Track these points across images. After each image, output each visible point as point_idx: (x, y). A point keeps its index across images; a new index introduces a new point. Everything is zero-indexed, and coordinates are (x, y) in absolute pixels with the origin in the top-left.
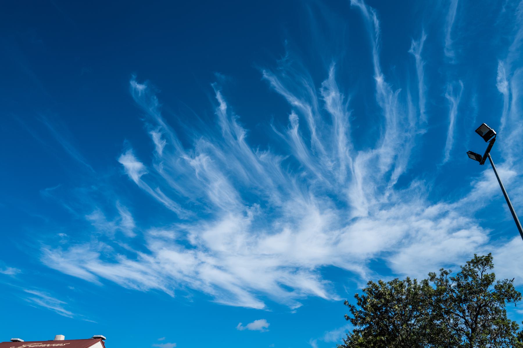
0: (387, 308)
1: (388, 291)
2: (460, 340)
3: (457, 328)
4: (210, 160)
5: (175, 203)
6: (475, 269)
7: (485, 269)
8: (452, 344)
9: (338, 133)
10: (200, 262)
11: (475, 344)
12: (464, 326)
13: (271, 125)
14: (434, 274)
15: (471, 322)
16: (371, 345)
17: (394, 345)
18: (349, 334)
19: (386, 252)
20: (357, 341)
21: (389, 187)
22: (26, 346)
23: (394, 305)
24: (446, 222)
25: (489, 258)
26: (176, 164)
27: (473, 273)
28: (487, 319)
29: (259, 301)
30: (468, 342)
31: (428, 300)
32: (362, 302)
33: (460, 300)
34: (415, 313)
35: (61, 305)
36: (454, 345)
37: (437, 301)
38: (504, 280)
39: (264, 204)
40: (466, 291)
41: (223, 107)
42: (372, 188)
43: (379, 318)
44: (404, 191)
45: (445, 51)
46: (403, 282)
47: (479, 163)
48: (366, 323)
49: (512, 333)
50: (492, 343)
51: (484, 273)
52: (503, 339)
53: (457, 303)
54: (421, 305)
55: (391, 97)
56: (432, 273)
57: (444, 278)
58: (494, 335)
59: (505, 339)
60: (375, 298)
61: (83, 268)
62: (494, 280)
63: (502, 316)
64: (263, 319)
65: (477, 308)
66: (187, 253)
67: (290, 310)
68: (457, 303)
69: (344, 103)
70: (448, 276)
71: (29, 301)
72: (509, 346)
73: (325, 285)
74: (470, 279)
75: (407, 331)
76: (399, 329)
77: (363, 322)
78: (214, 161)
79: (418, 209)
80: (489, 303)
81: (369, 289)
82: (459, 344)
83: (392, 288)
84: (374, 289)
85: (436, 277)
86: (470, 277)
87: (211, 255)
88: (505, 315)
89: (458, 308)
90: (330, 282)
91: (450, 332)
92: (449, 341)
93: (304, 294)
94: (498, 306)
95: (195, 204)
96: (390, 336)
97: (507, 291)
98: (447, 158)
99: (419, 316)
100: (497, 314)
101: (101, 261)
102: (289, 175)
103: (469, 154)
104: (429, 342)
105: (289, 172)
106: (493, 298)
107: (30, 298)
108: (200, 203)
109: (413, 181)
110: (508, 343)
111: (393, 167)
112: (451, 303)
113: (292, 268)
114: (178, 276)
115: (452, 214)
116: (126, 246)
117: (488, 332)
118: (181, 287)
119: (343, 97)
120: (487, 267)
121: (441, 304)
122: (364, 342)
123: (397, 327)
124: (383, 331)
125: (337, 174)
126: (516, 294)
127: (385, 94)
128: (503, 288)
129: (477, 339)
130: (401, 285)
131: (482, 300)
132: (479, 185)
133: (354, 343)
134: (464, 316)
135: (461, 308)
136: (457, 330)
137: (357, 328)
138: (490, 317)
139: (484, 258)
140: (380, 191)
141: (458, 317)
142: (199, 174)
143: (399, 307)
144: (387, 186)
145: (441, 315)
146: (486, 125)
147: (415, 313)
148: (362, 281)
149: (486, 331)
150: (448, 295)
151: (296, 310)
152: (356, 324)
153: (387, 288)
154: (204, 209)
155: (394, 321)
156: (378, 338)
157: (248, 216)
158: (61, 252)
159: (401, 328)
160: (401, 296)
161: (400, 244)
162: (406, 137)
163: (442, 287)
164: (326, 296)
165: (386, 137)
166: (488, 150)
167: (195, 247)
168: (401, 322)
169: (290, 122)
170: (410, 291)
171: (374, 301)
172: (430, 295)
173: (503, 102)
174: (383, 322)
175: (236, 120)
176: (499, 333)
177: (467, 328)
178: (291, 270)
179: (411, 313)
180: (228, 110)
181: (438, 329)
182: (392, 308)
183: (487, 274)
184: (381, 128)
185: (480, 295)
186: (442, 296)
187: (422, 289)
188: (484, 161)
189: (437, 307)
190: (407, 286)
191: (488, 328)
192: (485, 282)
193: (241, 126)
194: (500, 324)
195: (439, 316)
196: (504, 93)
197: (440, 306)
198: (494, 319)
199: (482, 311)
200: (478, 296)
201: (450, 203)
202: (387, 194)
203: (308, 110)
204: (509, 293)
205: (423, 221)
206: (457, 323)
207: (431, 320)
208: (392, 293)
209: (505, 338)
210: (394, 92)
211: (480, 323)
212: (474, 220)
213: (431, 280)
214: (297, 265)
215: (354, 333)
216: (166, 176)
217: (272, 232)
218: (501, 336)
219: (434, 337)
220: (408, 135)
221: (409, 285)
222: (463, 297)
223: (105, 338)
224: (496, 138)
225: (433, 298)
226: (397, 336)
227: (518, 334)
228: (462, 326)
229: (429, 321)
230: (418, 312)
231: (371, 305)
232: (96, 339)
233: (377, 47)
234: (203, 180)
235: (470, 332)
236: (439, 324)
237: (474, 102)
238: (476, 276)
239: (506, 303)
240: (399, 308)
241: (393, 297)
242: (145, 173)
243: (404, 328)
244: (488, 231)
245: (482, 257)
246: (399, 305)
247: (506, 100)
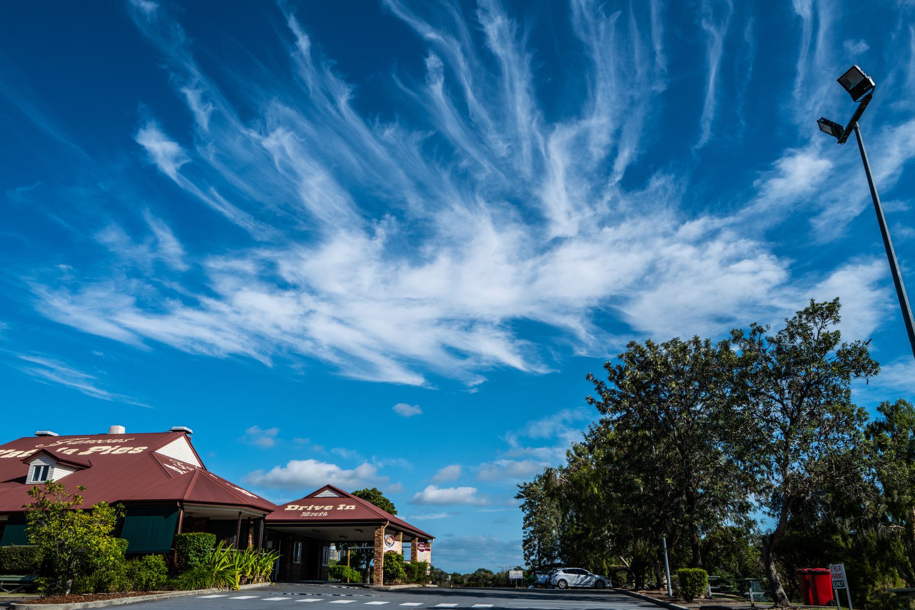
1: (661, 359)
2: (769, 436)
3: (769, 417)
5: (242, 212)
6: (809, 324)
7: (825, 324)
11: (794, 442)
12: (779, 415)
13: (394, 76)
16: (627, 444)
17: (665, 444)
18: (593, 426)
21: (610, 185)
22: (62, 443)
23: (671, 380)
24: (716, 248)
25: (834, 306)
26: (235, 145)
30: (783, 439)
32: (617, 375)
34: (704, 393)
35: (87, 380)
39: (400, 215)
40: (790, 359)
41: (304, 43)
43: (643, 400)
48: (621, 408)
50: (821, 441)
51: (823, 331)
52: (840, 434)
53: (772, 379)
54: (715, 382)
56: (737, 330)
59: (843, 435)
60: (638, 368)
61: (112, 322)
62: (838, 342)
63: (843, 399)
65: (805, 386)
69: (518, 36)
71: (31, 374)
73: (521, 347)
74: (799, 340)
75: (688, 422)
76: (675, 419)
77: (616, 407)
80: (824, 379)
81: (629, 354)
82: (769, 442)
83: (669, 354)
84: (637, 355)
85: (743, 337)
86: (798, 338)
87: (323, 300)
88: (848, 398)
90: (529, 343)
91: (757, 424)
94: (838, 383)
95: (278, 215)
97: (856, 360)
98: (706, 136)
100: (835, 396)
101: (139, 310)
102: (437, 166)
104: (721, 439)
106: (832, 371)
107: (33, 369)
109: (654, 178)
110: (848, 442)
111: (614, 152)
112: (763, 379)
114: (273, 333)
115: (728, 235)
116: (177, 286)
120: (829, 322)
121: (747, 381)
123: (672, 416)
124: (649, 422)
126: (871, 365)
128: (850, 355)
129: (798, 434)
131: (813, 373)
134: (782, 399)
136: (768, 421)
137: (608, 416)
138: (822, 401)
140: (596, 194)
141: (772, 401)
143: (677, 384)
144: (607, 183)
145: (745, 398)
146: (859, 69)
147: (704, 393)
149: (814, 422)
150: (760, 366)
151: (476, 389)
152: (604, 412)
153: (660, 353)
155: (668, 406)
156: (639, 433)
158: (69, 296)
159: (678, 417)
160: (682, 367)
163: (751, 353)
164: (523, 366)
165: (599, 98)
166: (856, 117)
168: (680, 408)
170: (698, 358)
171: (637, 374)
174: (650, 408)
176: (835, 425)
177: (784, 418)
178: (463, 324)
179: (697, 393)
180: (313, 50)
182: (667, 386)
183: (828, 332)
186: (749, 368)
187: (717, 357)
189: (741, 384)
190: (693, 350)
191: (818, 417)
192: (822, 345)
194: (838, 411)
199: (811, 391)
200: (808, 367)
201: (721, 216)
202: (608, 197)
204: (858, 363)
205: (678, 246)
206: (770, 409)
207: (728, 406)
209: (843, 434)
210: (608, 15)
211: (805, 410)
212: (763, 243)
214: (471, 316)
216: (218, 165)
217: (418, 261)
218: (837, 430)
221: (698, 348)
223: (191, 431)
224: (874, 95)
226: (671, 430)
228: (776, 415)
230: (709, 393)
231: (632, 381)
232: (177, 433)
235: (788, 424)
238: (808, 335)
239: (852, 378)
241: (669, 368)
242: (186, 161)
243: (684, 417)
245: (824, 305)
246: (679, 382)
247: (807, 28)
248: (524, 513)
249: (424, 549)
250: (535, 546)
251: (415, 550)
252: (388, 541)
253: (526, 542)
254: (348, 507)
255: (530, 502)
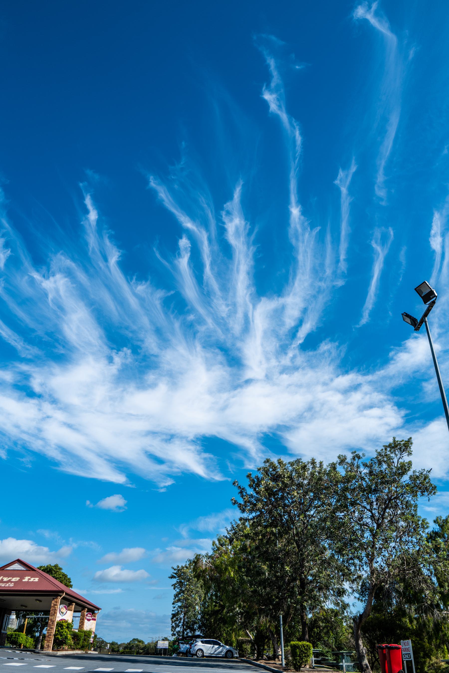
0: (284, 494)
3: (362, 522)
4: (70, 283)
5: (16, 334)
6: (392, 455)
7: (402, 455)
8: (353, 541)
9: (238, 271)
10: (45, 416)
11: (379, 542)
12: (369, 521)
13: (155, 249)
14: (345, 456)
15: (378, 516)
17: (286, 539)
18: (233, 523)
19: (283, 425)
20: (243, 532)
21: (293, 346)
23: (293, 490)
27: (389, 460)
28: (396, 513)
29: (119, 474)
30: (371, 539)
31: (333, 487)
33: (370, 490)
34: (316, 502)
36: (355, 542)
37: (344, 490)
38: (421, 470)
39: (135, 350)
40: (378, 480)
41: (93, 216)
42: (273, 345)
44: (311, 353)
45: (376, 188)
46: (306, 464)
47: (414, 328)
48: (256, 509)
49: (421, 532)
50: (397, 542)
51: (400, 460)
52: (410, 538)
53: (365, 493)
55: (307, 235)
56: (342, 455)
57: (355, 462)
58: (400, 533)
59: (412, 539)
63: (413, 512)
64: (115, 495)
66: (29, 402)
67: (158, 488)
68: (365, 493)
69: (249, 234)
70: (360, 461)
72: (415, 546)
73: (205, 459)
74: (385, 466)
75: (304, 523)
76: (295, 520)
77: (253, 508)
78: (74, 285)
79: (326, 377)
80: (400, 496)
81: (265, 468)
83: (293, 470)
84: (271, 470)
85: (346, 461)
86: (384, 464)
87: (60, 409)
88: (415, 511)
89: (366, 499)
90: (212, 456)
91: (353, 527)
92: (351, 537)
93: (178, 468)
95: (44, 340)
96: (283, 527)
98: (365, 320)
99: (321, 506)
102: (172, 316)
103: (404, 316)
105: (173, 312)
108: (50, 339)
109: (323, 343)
110: (415, 544)
111: (300, 322)
112: (359, 493)
113: (166, 434)
115: (366, 388)
117: (395, 529)
118: (16, 446)
119: (248, 227)
120: (405, 454)
121: (348, 494)
122: (251, 534)
123: (292, 517)
124: (276, 521)
125: (231, 322)
126: (431, 487)
127: (300, 230)
128: (418, 479)
129: (381, 536)
130: (304, 467)
132: (399, 357)
133: (239, 534)
134: (371, 509)
135: (369, 499)
136: (361, 525)
137: (245, 515)
138: (399, 512)
139: (404, 442)
141: (364, 510)
142: (52, 301)
143: (298, 493)
144: (291, 344)
145: (346, 506)
146: (428, 284)
147: (316, 502)
148: (250, 459)
150: (357, 483)
154: (55, 347)
155: (291, 510)
156: (268, 530)
157: (114, 363)
159: (297, 519)
160: (302, 481)
161: (301, 418)
162: (319, 287)
164: (205, 473)
166: (426, 315)
167: (40, 396)
169: (179, 249)
170: (314, 475)
171: (270, 484)
172: (337, 482)
173: (434, 260)
175: (108, 236)
176: (407, 531)
177: (373, 523)
178: (164, 437)
180: (99, 222)
181: (339, 523)
182: (290, 495)
184: (291, 271)
185: (393, 485)
186: (350, 484)
187: (328, 474)
188: (419, 326)
189: (343, 496)
190: (311, 469)
191: (396, 524)
193: (114, 245)
195: (344, 507)
196: (436, 250)
197: (345, 495)
198: (403, 514)
199: (391, 504)
200: (390, 486)
201: (364, 375)
203: (203, 236)
204: (423, 485)
205: (330, 393)
206: (363, 516)
208: (292, 476)
209: (412, 537)
210: (311, 229)
212: (389, 397)
213: (340, 464)
214: (172, 432)
215: (240, 522)
219: (334, 532)
220: (323, 285)
221: (314, 467)
222: (373, 487)
225: (339, 486)
227: (428, 534)
228: (367, 521)
229: (331, 512)
230: (320, 501)
233: (296, 169)
234: (57, 309)
235: (375, 528)
236: (341, 516)
237: (402, 256)
239: (419, 496)
240: (298, 495)
241: (293, 481)
243: (301, 519)
244: (403, 412)
245: (402, 442)
246: (299, 492)
247: (438, 258)
248: (175, 591)
249: (91, 618)
250: (181, 619)
251: (83, 619)
252: (62, 610)
253: (174, 615)
254: (32, 580)
255: (181, 582)
